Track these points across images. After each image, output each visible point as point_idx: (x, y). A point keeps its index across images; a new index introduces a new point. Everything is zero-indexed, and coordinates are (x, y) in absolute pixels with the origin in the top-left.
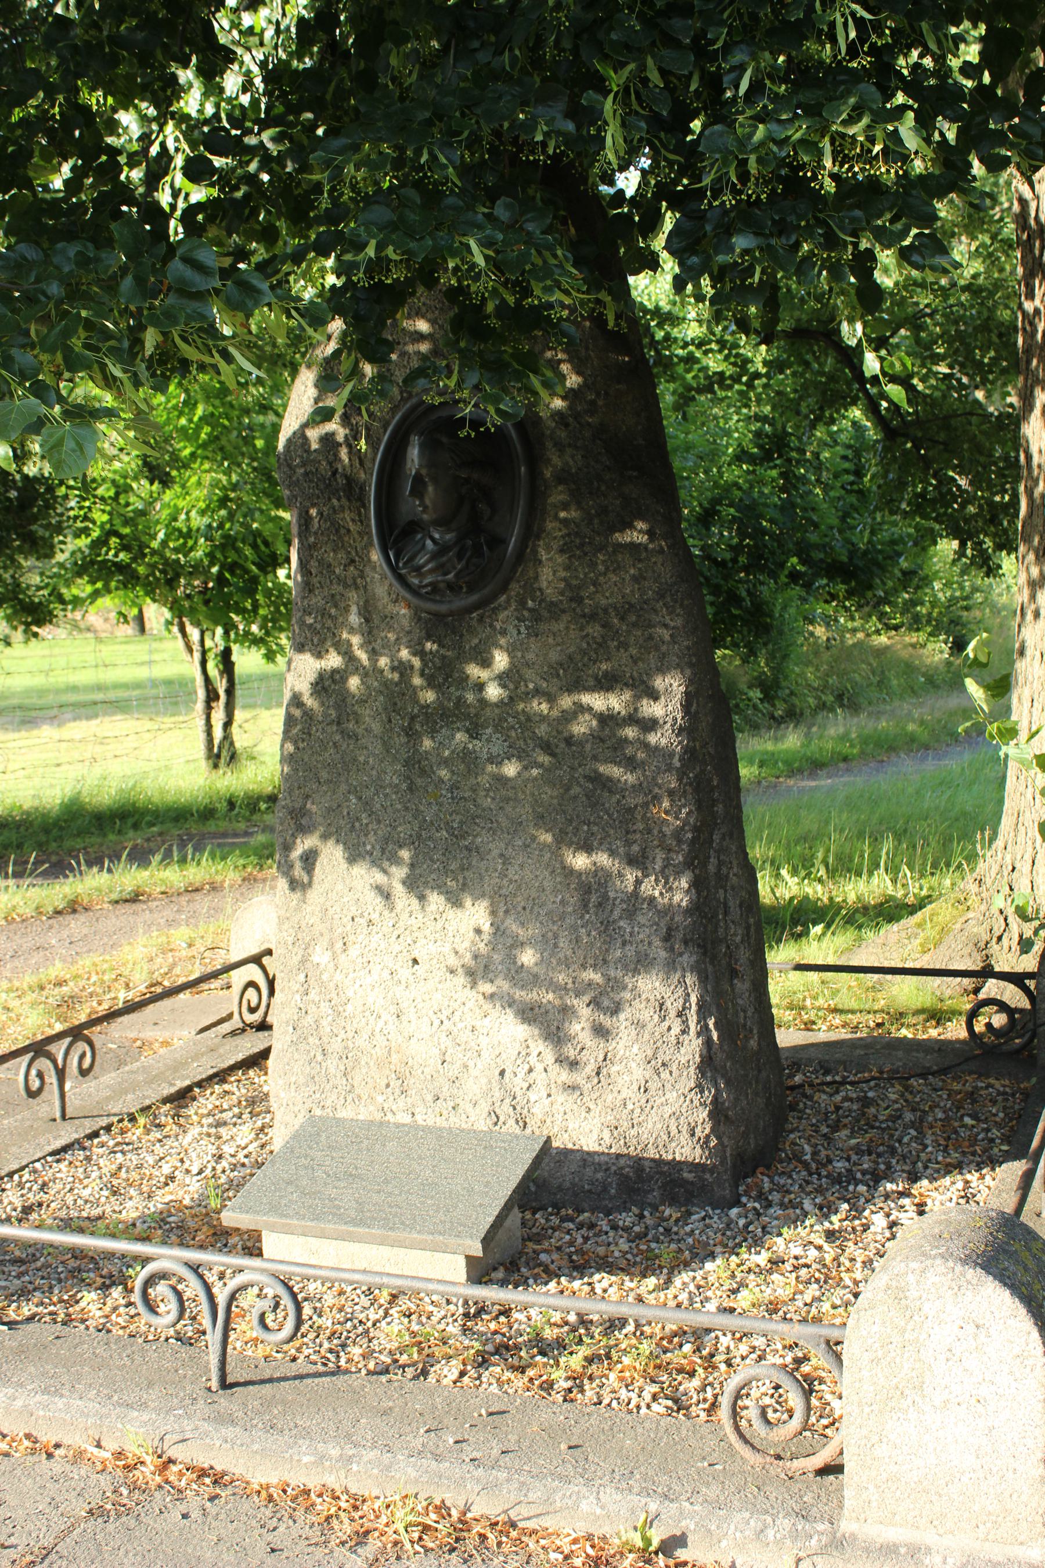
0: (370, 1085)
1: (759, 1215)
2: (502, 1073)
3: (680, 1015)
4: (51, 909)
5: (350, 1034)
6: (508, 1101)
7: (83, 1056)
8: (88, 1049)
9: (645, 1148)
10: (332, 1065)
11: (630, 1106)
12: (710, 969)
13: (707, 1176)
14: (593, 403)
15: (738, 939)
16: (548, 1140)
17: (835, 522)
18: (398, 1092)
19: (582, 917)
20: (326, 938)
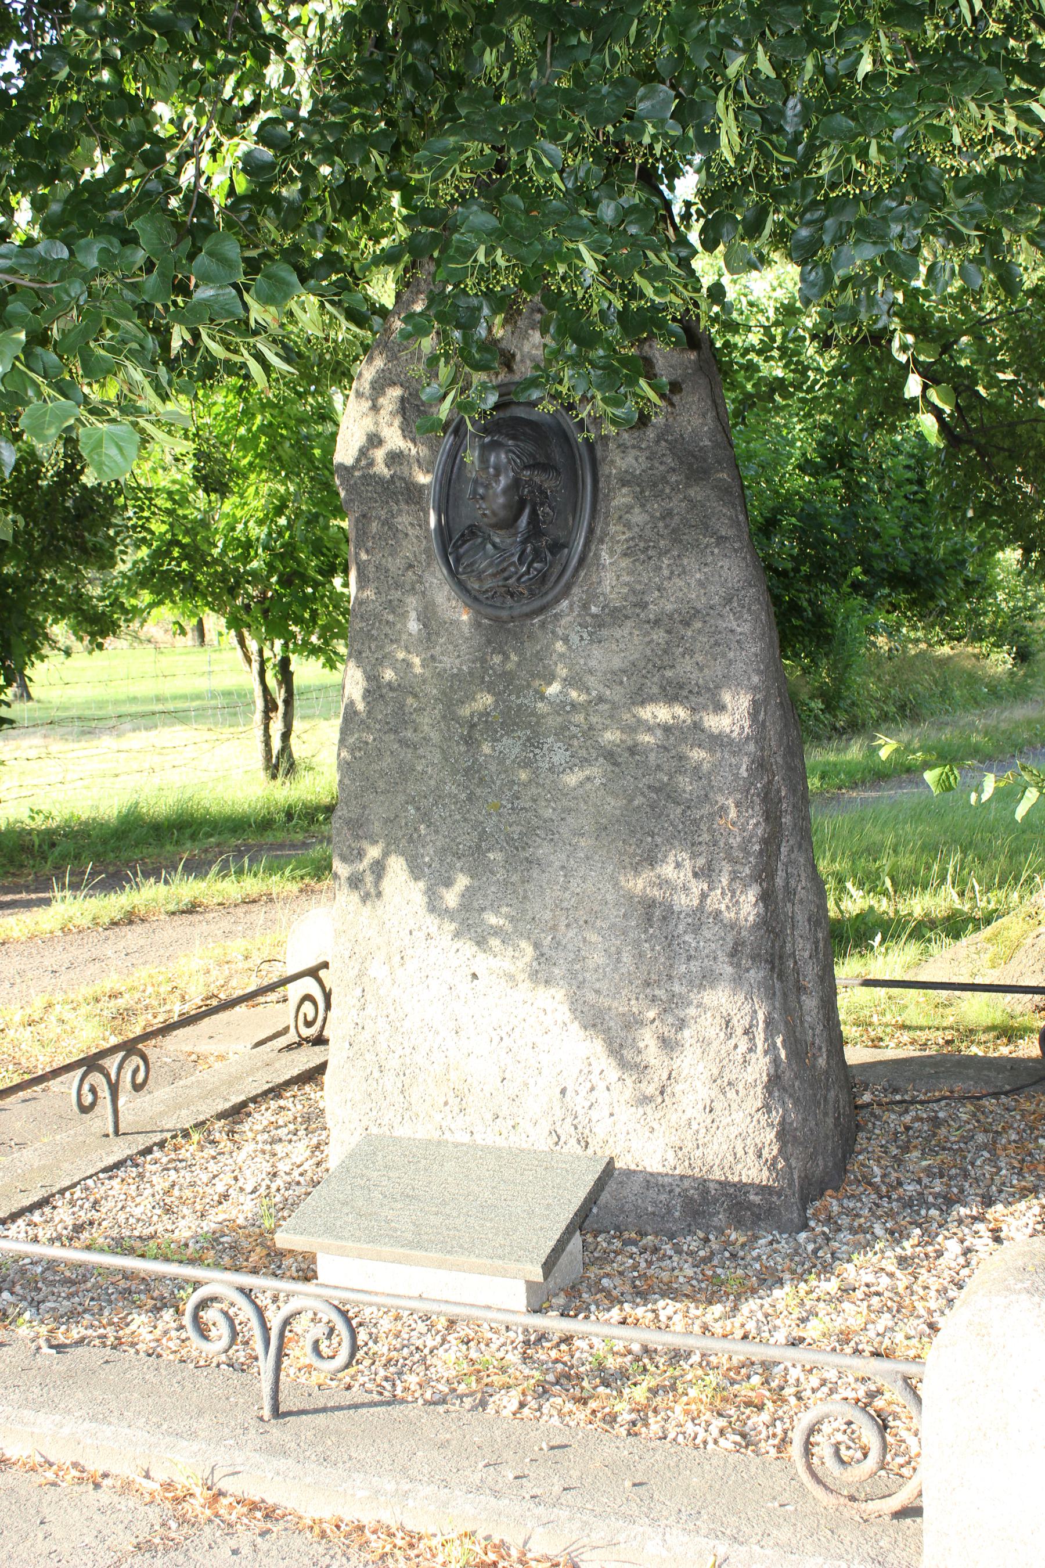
1: (828, 1239)
2: (563, 1092)
3: (746, 1032)
4: (107, 920)
5: (408, 1051)
7: (136, 1071)
11: (695, 1126)
12: (778, 985)
13: (775, 1199)
15: (806, 954)
18: (456, 1110)
19: (646, 931)
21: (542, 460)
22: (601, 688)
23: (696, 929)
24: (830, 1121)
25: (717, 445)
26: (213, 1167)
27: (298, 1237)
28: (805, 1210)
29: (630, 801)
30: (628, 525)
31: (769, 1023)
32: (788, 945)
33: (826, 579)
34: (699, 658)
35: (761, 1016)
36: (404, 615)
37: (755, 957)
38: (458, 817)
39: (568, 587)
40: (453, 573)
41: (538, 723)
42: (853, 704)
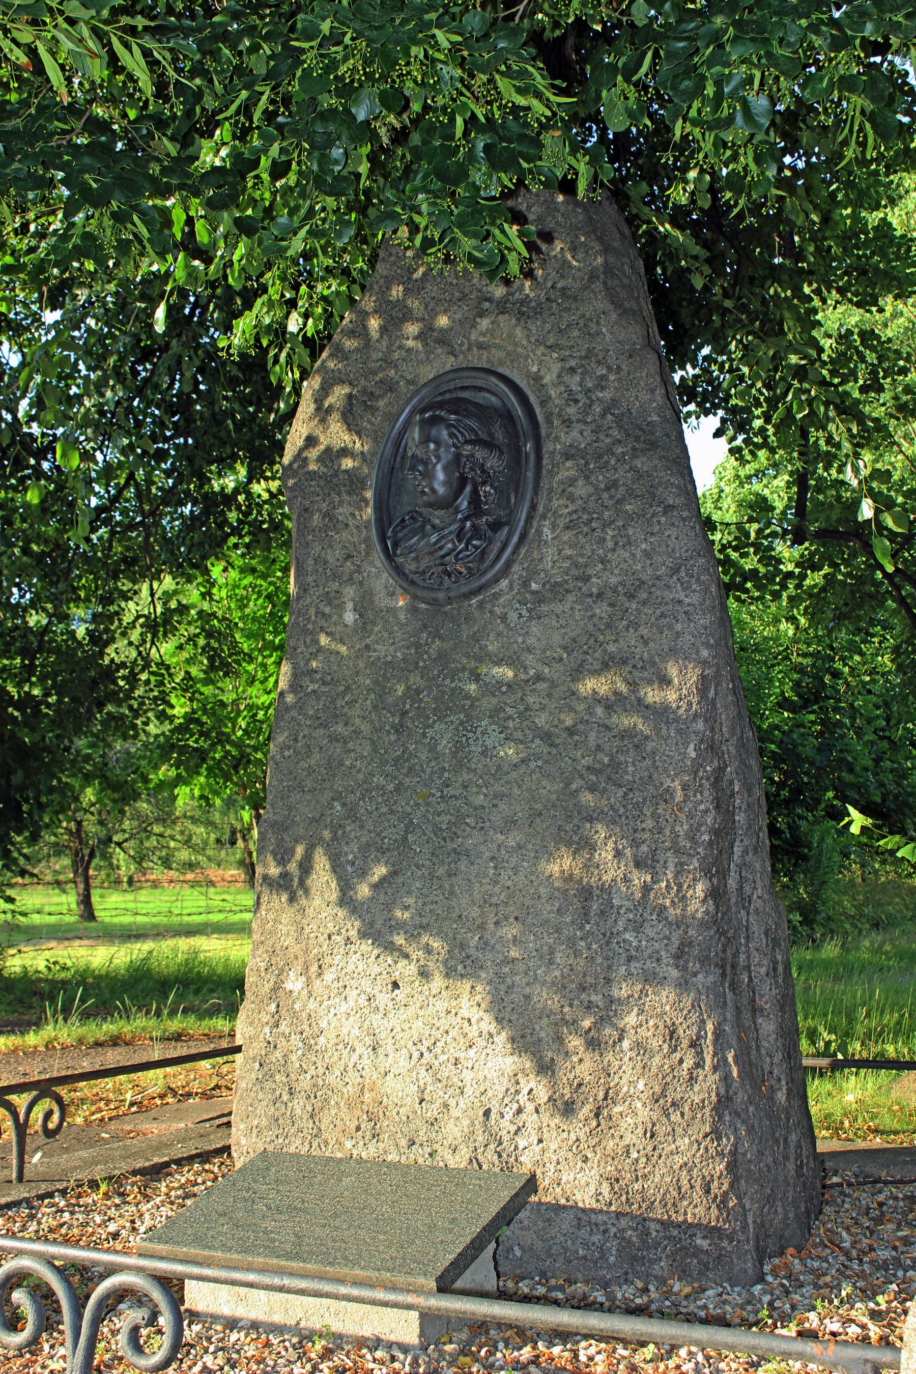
0: (339, 1129)
1: (787, 1292)
2: (487, 1113)
3: (693, 1045)
4: (91, 1040)
5: (321, 1071)
6: (492, 1146)
7: (48, 1115)
8: (56, 1108)
9: (651, 1207)
10: (299, 1106)
11: (634, 1155)
12: (729, 995)
13: (725, 1244)
14: (603, 378)
15: (763, 970)
16: (531, 1184)
17: (870, 763)
18: (368, 1135)
19: (581, 928)
20: (301, 960)
21: (484, 437)
22: (540, 667)
23: (638, 926)
24: (791, 1166)
25: (665, 420)
26: (112, 1212)
27: (161, 1246)
28: (762, 1265)
29: (567, 785)
30: (571, 498)
31: (718, 1034)
32: (742, 957)
33: (803, 803)
34: (644, 631)
35: (710, 1027)
36: (341, 607)
37: (704, 960)
38: (384, 810)
39: (509, 564)
40: (389, 556)
41: (472, 705)
42: (829, 918)
